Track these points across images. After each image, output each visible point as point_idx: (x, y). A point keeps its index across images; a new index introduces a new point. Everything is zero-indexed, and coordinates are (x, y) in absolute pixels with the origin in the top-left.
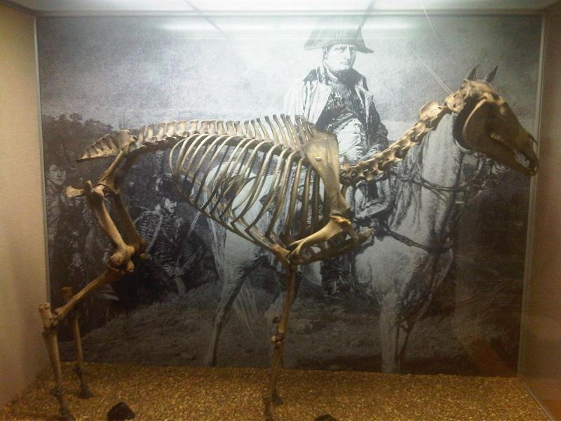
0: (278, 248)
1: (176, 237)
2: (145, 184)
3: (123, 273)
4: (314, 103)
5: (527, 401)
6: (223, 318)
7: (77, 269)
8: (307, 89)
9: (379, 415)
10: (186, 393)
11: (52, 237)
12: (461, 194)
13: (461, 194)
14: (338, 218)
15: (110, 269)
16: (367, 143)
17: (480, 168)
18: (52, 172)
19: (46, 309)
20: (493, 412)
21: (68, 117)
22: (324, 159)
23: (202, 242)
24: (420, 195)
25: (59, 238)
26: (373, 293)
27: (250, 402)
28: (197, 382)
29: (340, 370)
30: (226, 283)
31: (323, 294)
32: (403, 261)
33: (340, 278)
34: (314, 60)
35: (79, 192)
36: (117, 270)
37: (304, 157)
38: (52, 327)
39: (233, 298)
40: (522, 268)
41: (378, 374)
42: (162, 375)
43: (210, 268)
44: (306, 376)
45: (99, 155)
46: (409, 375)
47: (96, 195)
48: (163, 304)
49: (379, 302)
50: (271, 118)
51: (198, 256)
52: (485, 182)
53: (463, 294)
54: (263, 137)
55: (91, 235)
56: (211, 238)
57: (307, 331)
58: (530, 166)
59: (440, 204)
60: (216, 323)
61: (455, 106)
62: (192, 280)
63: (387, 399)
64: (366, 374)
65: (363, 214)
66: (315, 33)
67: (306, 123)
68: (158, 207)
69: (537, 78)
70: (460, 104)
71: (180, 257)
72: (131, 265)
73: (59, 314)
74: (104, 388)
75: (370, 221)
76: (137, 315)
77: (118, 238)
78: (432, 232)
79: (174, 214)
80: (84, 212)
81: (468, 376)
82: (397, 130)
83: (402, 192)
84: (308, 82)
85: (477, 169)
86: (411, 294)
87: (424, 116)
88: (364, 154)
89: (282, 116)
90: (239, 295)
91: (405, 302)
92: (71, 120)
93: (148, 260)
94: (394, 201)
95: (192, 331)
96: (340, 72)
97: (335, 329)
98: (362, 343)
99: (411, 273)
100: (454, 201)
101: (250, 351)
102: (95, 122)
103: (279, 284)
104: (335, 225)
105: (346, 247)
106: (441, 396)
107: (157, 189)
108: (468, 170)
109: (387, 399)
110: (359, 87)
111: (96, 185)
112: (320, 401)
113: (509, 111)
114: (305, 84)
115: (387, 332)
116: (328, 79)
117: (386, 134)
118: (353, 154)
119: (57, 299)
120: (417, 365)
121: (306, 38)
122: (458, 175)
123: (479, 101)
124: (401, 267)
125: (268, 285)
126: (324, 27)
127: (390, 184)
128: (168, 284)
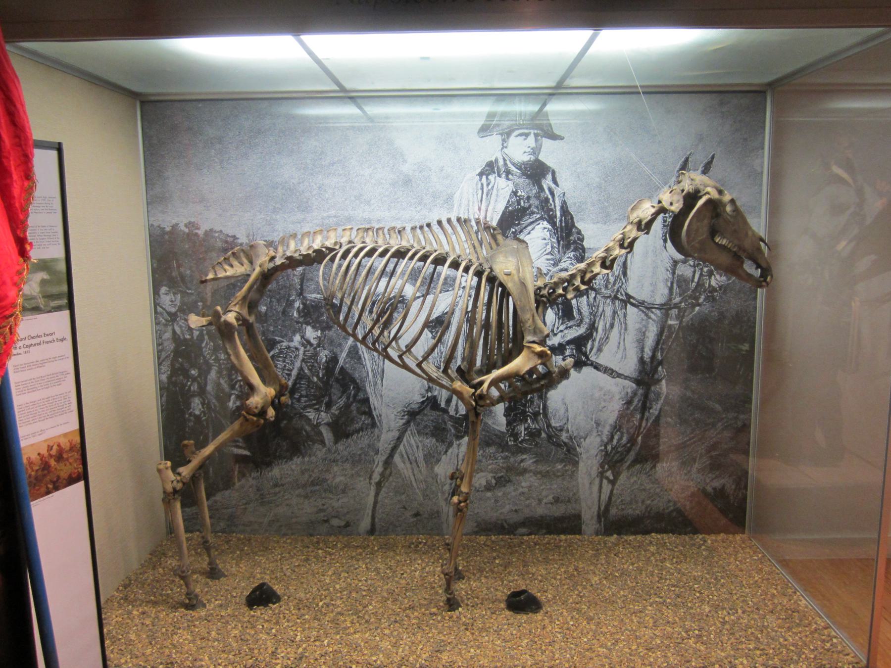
0: (460, 386)
1: (321, 375)
2: (280, 309)
3: (262, 421)
4: (492, 202)
5: (761, 563)
6: (382, 475)
7: (198, 418)
8: (482, 185)
9: (585, 588)
10: (341, 569)
11: (164, 377)
12: (674, 312)
13: (674, 312)
14: (535, 346)
15: (245, 417)
16: (559, 251)
17: (696, 280)
18: (162, 296)
19: (167, 468)
20: (722, 577)
21: (182, 227)
22: (514, 272)
23: (353, 381)
24: (625, 316)
25: (174, 379)
26: (571, 438)
27: (423, 578)
28: (354, 554)
29: (530, 534)
30: (384, 431)
31: (507, 442)
32: (606, 397)
33: (529, 421)
34: (490, 148)
35: (204, 321)
36: (255, 419)
37: (488, 270)
38: (175, 491)
39: (394, 449)
40: (751, 399)
41: (577, 536)
42: (308, 547)
43: (364, 413)
44: (489, 543)
45: (228, 274)
46: (615, 536)
47: (227, 324)
48: (306, 459)
49: (578, 449)
50: (445, 223)
51: (348, 398)
52: (703, 297)
53: (670, 437)
54: (435, 246)
55: (213, 375)
56: (365, 374)
57: (489, 487)
58: (761, 276)
59: (650, 325)
60: (373, 482)
61: (671, 204)
62: (341, 430)
63: (592, 568)
64: (563, 537)
65: (555, 341)
66: (491, 115)
67: (487, 228)
68: (297, 338)
69: (762, 167)
70: (678, 201)
71: (326, 399)
72: (271, 412)
73: (183, 474)
74: (237, 565)
75: (566, 349)
76: (276, 472)
77: (255, 379)
78: (642, 361)
79: (318, 345)
80: (203, 345)
81: (686, 534)
82: (598, 237)
83: (603, 311)
84: (484, 177)
85: (693, 281)
86: (616, 437)
87: (634, 217)
88: (555, 264)
89: (459, 220)
90: (402, 445)
91: (609, 448)
92: (187, 230)
93: (287, 406)
94: (594, 323)
95: (344, 491)
96: (523, 163)
97: (523, 484)
98: (557, 500)
99: (617, 412)
100: (666, 321)
101: (417, 515)
102: (216, 232)
103: (453, 431)
104: (532, 355)
105: (542, 383)
106: (656, 561)
107: (295, 314)
108: (682, 282)
109: (592, 568)
110: (547, 182)
111: (226, 311)
112: (509, 573)
113: (736, 210)
114: (481, 180)
115: (588, 487)
116: (508, 172)
117: (582, 240)
118: (543, 263)
119: (175, 454)
120: (619, 525)
121: (480, 122)
122: (671, 289)
123: (701, 197)
124: (603, 404)
125: (438, 432)
126: (502, 108)
127: (588, 302)
128: (313, 433)
